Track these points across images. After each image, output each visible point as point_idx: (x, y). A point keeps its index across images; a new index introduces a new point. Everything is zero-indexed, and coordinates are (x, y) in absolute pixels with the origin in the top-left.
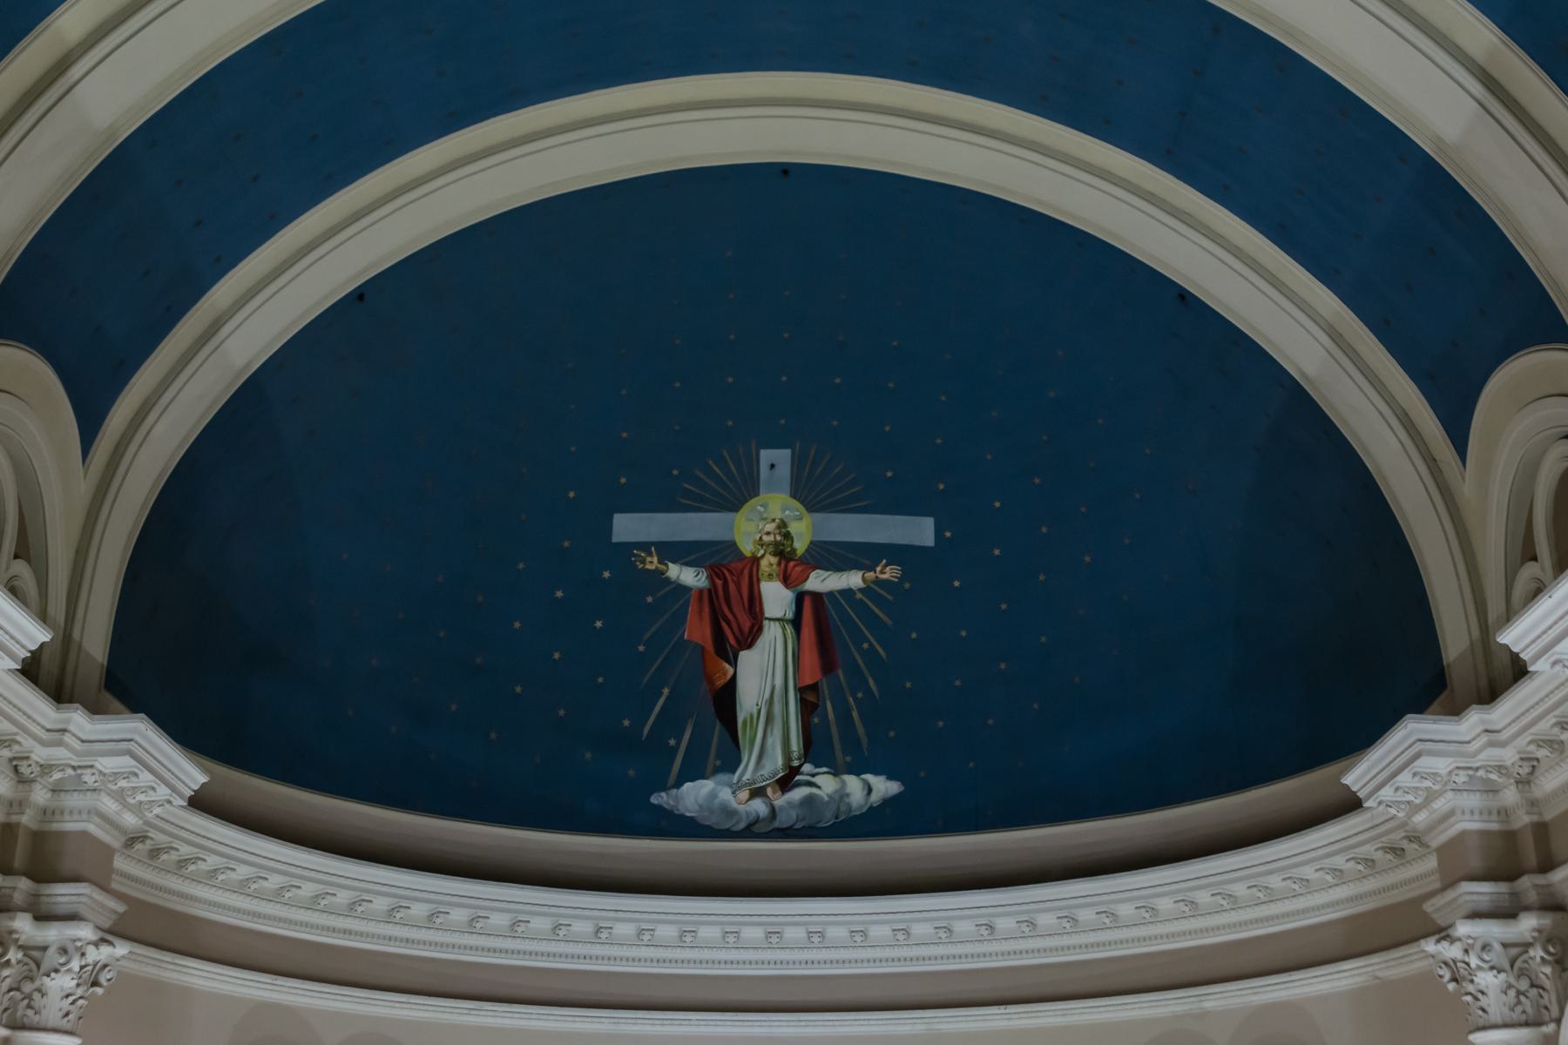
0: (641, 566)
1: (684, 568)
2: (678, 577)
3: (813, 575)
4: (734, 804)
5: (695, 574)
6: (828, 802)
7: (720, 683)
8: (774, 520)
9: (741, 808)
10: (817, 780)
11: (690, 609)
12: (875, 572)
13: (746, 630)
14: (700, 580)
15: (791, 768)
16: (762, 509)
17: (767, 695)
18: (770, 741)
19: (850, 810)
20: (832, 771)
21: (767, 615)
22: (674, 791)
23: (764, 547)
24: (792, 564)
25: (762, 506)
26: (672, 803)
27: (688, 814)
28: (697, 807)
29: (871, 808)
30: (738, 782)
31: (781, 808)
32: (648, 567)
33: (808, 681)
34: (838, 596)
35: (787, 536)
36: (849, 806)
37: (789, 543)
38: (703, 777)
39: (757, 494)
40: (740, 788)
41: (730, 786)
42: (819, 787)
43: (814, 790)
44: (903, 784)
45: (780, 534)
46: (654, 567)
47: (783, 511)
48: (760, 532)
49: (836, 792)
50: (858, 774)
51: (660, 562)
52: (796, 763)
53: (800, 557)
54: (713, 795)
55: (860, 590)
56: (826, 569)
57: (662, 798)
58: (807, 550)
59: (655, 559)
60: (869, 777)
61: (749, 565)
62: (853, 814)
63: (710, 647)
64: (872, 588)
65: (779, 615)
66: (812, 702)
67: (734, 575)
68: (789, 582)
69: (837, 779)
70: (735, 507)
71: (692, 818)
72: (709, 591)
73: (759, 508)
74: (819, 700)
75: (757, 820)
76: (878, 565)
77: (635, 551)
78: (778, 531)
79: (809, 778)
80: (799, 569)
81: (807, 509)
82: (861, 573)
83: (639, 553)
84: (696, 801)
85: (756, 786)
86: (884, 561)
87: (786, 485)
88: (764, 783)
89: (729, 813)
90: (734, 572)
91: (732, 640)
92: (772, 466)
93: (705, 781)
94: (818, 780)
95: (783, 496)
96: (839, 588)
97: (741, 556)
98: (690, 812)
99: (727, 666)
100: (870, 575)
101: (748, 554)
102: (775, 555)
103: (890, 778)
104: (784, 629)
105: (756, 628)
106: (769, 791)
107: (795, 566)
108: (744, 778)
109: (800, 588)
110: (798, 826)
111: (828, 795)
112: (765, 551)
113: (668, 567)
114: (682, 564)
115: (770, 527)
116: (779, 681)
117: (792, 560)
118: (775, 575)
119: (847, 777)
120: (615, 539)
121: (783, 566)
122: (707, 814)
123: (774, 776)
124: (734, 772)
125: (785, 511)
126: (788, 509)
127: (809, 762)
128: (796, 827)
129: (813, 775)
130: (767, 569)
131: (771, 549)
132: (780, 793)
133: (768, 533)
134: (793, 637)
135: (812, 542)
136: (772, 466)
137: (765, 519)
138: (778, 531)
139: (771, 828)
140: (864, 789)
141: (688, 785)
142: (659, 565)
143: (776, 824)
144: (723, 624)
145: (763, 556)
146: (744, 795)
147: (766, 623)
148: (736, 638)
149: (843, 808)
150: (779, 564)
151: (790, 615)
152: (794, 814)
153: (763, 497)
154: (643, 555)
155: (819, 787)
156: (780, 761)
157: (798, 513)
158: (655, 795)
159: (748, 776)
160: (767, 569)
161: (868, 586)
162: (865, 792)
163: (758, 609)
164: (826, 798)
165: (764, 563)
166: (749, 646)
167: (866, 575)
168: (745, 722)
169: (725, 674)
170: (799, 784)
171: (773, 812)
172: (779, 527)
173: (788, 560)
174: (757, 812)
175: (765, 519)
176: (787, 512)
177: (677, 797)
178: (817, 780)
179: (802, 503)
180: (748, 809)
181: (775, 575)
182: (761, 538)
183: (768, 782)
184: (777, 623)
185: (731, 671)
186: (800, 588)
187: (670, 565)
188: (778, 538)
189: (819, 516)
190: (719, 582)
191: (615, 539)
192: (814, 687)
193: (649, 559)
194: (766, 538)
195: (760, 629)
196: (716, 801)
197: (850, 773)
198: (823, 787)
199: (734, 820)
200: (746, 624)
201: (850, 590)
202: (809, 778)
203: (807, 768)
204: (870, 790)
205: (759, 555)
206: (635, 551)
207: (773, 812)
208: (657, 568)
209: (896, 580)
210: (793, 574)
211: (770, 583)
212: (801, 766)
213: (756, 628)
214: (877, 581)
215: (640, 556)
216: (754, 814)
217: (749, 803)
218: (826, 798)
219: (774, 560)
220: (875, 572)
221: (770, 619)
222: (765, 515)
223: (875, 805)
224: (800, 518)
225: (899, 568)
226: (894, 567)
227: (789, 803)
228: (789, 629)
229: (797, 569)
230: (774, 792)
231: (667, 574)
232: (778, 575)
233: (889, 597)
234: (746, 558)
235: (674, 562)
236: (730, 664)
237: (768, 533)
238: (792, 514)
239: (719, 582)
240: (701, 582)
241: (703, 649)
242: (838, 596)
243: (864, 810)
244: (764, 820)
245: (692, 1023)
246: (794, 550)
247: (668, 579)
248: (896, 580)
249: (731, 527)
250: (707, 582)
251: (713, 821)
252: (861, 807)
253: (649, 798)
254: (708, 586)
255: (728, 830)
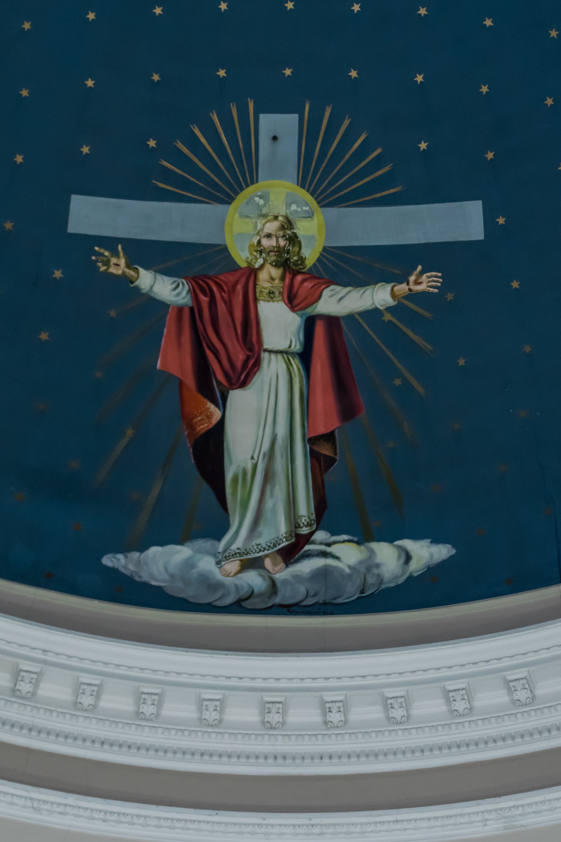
0: (103, 268)
1: (159, 277)
2: (152, 287)
3: (327, 293)
4: (218, 575)
5: (174, 286)
6: (350, 576)
7: (203, 427)
8: (276, 218)
9: (228, 580)
10: (334, 549)
11: (165, 330)
12: (408, 284)
13: (239, 364)
14: (178, 294)
15: (298, 536)
16: (262, 202)
17: (266, 446)
18: (269, 504)
19: (381, 582)
20: (355, 539)
21: (266, 346)
22: (135, 555)
23: (264, 255)
24: (299, 278)
25: (261, 197)
26: (132, 567)
27: (154, 583)
28: (167, 577)
29: (411, 578)
30: (225, 551)
31: (285, 582)
32: (113, 270)
33: (321, 430)
34: (361, 321)
35: (294, 239)
36: (380, 578)
37: (296, 249)
38: (181, 542)
39: (254, 181)
40: (227, 558)
41: (215, 555)
42: (337, 558)
43: (330, 562)
44: (454, 546)
45: (284, 236)
46: (120, 272)
47: (288, 205)
48: (258, 234)
49: (361, 562)
50: (391, 540)
51: (128, 266)
52: (305, 531)
53: (310, 269)
54: (189, 564)
55: (389, 309)
56: (345, 285)
57: (119, 560)
58: (319, 260)
59: (122, 262)
60: (407, 543)
61: (243, 280)
62: (383, 587)
63: (190, 381)
64: (403, 304)
65: (283, 346)
66: (325, 456)
67: (224, 291)
68: (295, 302)
69: (362, 548)
70: (228, 200)
71: (159, 588)
72: (192, 309)
73: (257, 199)
74: (336, 454)
75: (251, 595)
76: (410, 274)
77: (96, 248)
78: (281, 233)
79: (323, 548)
80: (308, 285)
81: (318, 203)
82: (389, 287)
83: (102, 251)
84: (166, 569)
85: (249, 557)
86: (420, 267)
87: (292, 168)
88: (261, 554)
89: (216, 586)
90: (225, 288)
91: (221, 377)
92: (275, 138)
93: (178, 548)
94: (334, 549)
95: (288, 184)
96: (362, 309)
97: (234, 267)
98: (156, 580)
99: (212, 407)
100: (402, 288)
101: (243, 265)
102: (277, 265)
103: (436, 541)
104: (289, 364)
105: (251, 362)
106: (268, 563)
107: (303, 281)
108: (234, 547)
109: (310, 311)
110: (310, 602)
111: (349, 567)
112: (265, 260)
113: (138, 273)
114: (157, 271)
115: (272, 227)
116: (282, 430)
117: (299, 272)
118: (277, 293)
119: (375, 545)
120: (71, 229)
121: (287, 281)
122: (180, 584)
123: (275, 546)
124: (219, 538)
125: (290, 205)
126: (294, 202)
127: (323, 529)
128: (305, 603)
129: (329, 545)
130: (267, 285)
131: (272, 258)
132: (282, 565)
133: (269, 236)
134: (300, 375)
135: (325, 249)
136: (275, 138)
137: (265, 216)
138: (281, 233)
139: (270, 604)
140: (399, 557)
141: (154, 550)
142: (127, 270)
143: (278, 600)
144: (210, 355)
145: (262, 267)
146: (233, 566)
147: (265, 356)
148: (226, 375)
149: (371, 580)
150: (283, 279)
151: (297, 347)
152: (302, 589)
153: (262, 185)
154: (106, 254)
155: (337, 558)
156: (283, 528)
157: (307, 208)
158: (109, 555)
159: (239, 544)
160: (267, 285)
161: (399, 302)
162: (402, 560)
163: (254, 339)
164: (347, 570)
165: (263, 276)
166: (243, 384)
167: (395, 289)
168: (235, 479)
169: (209, 417)
170: (308, 555)
171: (273, 586)
172: (282, 228)
173: (296, 273)
174: (249, 585)
175: (265, 216)
176: (294, 207)
177: (139, 561)
178: (334, 549)
179: (312, 194)
180: (238, 582)
181: (277, 293)
182: (259, 242)
183: (266, 552)
184: (280, 357)
185: (217, 414)
186: (310, 311)
187: (141, 270)
188: (282, 242)
189: (333, 211)
190: (204, 299)
191: (71, 229)
192: (329, 437)
193: (114, 260)
194: (266, 243)
195: (257, 364)
196: (194, 571)
197: (380, 539)
198: (343, 558)
199: (218, 595)
200: (240, 357)
201: (376, 310)
202: (323, 548)
203: (321, 535)
204: (408, 558)
205: (257, 266)
206: (96, 248)
207: (273, 586)
208: (124, 272)
209: (436, 291)
210: (299, 293)
211: (271, 303)
212: (312, 533)
213: (251, 362)
214: (412, 296)
215: (103, 255)
216: (246, 589)
217: (240, 575)
218: (347, 570)
219: (276, 273)
220: (408, 284)
221: (270, 352)
222: (265, 211)
223: (416, 574)
224: (310, 216)
225: (440, 274)
226: (433, 273)
227: (297, 578)
228: (296, 364)
229: (306, 284)
230: (275, 564)
231: (136, 283)
232: (281, 293)
233: (427, 314)
234: (239, 268)
235: (146, 268)
236: (217, 405)
237: (269, 236)
238: (299, 209)
239: (204, 299)
240: (180, 297)
241: (181, 383)
242: (361, 321)
243: (401, 581)
244: (260, 595)
245: (149, 822)
246: (302, 260)
247: (137, 288)
248: (436, 291)
249: (221, 225)
250: (189, 297)
251: (189, 594)
252: (396, 578)
253: (102, 556)
254: (190, 304)
255: (209, 604)
